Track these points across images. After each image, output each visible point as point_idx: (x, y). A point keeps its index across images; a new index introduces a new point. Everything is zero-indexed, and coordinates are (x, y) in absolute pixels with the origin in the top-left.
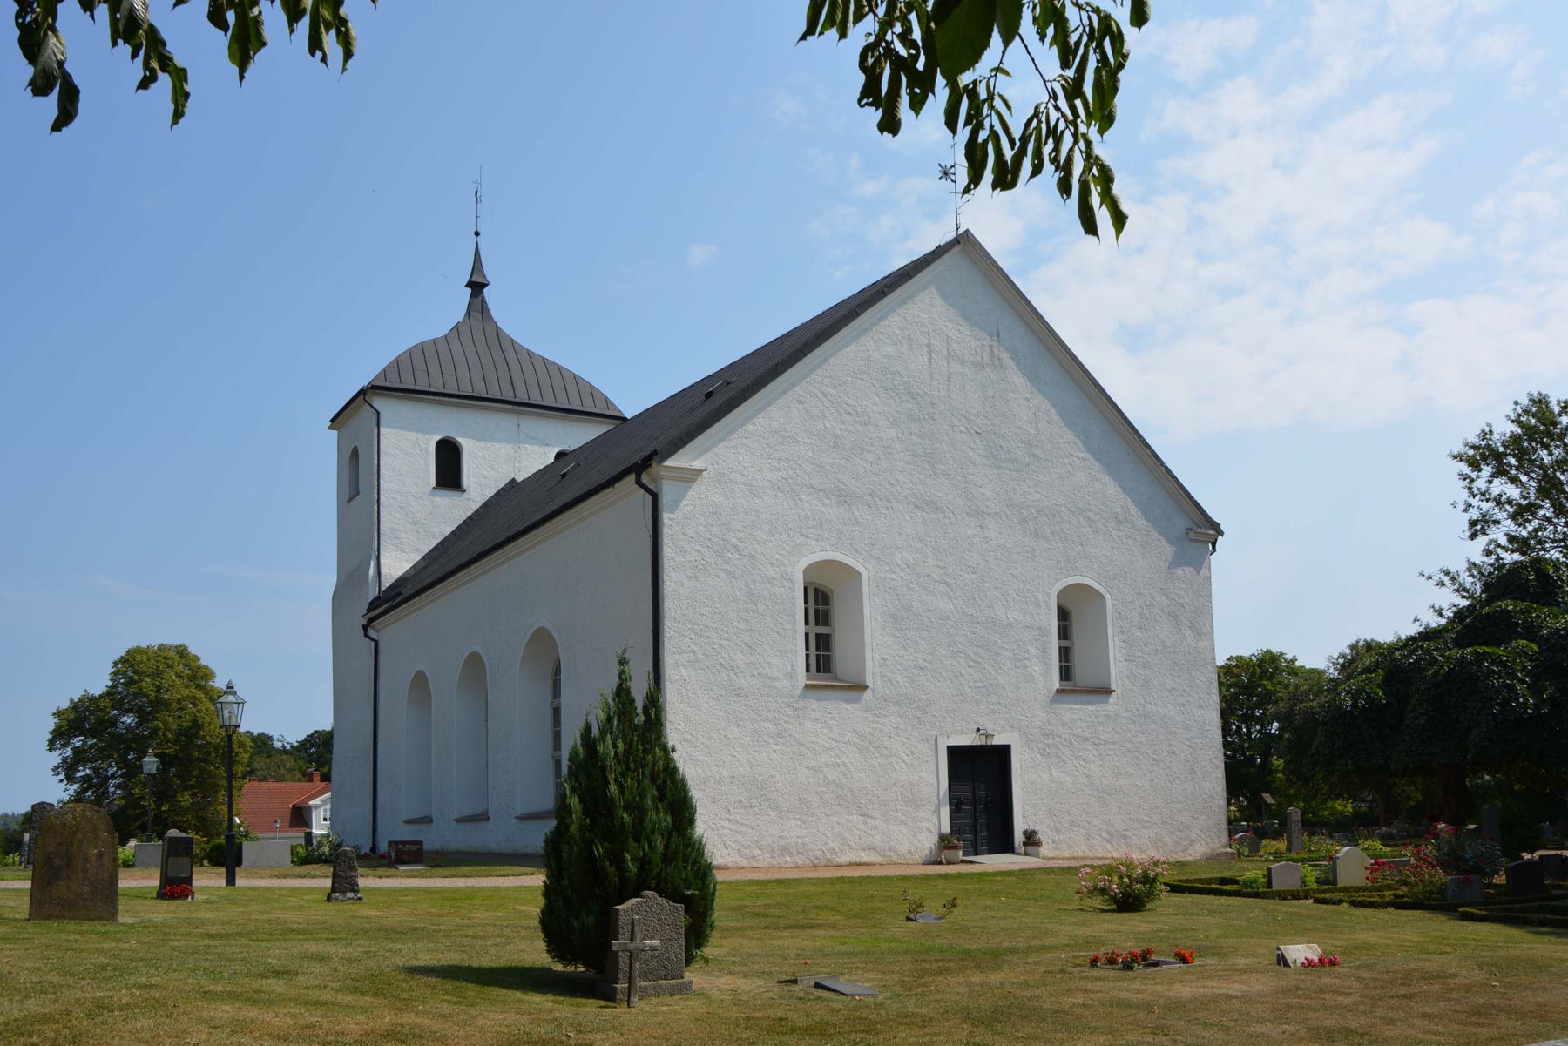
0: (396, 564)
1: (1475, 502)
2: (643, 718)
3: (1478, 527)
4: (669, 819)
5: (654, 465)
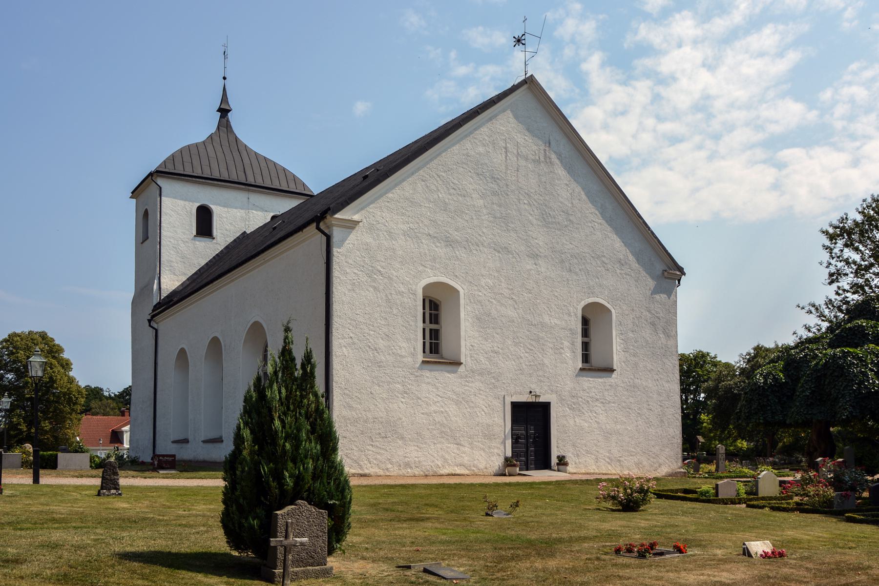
0: (170, 282)
1: (833, 262)
2: (301, 372)
3: (834, 277)
4: (319, 447)
5: (328, 217)
